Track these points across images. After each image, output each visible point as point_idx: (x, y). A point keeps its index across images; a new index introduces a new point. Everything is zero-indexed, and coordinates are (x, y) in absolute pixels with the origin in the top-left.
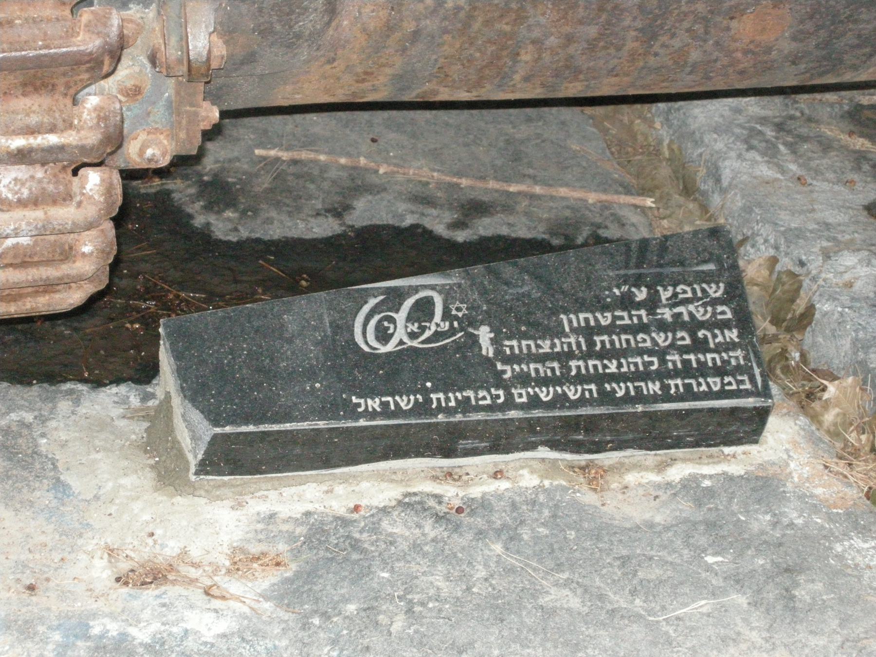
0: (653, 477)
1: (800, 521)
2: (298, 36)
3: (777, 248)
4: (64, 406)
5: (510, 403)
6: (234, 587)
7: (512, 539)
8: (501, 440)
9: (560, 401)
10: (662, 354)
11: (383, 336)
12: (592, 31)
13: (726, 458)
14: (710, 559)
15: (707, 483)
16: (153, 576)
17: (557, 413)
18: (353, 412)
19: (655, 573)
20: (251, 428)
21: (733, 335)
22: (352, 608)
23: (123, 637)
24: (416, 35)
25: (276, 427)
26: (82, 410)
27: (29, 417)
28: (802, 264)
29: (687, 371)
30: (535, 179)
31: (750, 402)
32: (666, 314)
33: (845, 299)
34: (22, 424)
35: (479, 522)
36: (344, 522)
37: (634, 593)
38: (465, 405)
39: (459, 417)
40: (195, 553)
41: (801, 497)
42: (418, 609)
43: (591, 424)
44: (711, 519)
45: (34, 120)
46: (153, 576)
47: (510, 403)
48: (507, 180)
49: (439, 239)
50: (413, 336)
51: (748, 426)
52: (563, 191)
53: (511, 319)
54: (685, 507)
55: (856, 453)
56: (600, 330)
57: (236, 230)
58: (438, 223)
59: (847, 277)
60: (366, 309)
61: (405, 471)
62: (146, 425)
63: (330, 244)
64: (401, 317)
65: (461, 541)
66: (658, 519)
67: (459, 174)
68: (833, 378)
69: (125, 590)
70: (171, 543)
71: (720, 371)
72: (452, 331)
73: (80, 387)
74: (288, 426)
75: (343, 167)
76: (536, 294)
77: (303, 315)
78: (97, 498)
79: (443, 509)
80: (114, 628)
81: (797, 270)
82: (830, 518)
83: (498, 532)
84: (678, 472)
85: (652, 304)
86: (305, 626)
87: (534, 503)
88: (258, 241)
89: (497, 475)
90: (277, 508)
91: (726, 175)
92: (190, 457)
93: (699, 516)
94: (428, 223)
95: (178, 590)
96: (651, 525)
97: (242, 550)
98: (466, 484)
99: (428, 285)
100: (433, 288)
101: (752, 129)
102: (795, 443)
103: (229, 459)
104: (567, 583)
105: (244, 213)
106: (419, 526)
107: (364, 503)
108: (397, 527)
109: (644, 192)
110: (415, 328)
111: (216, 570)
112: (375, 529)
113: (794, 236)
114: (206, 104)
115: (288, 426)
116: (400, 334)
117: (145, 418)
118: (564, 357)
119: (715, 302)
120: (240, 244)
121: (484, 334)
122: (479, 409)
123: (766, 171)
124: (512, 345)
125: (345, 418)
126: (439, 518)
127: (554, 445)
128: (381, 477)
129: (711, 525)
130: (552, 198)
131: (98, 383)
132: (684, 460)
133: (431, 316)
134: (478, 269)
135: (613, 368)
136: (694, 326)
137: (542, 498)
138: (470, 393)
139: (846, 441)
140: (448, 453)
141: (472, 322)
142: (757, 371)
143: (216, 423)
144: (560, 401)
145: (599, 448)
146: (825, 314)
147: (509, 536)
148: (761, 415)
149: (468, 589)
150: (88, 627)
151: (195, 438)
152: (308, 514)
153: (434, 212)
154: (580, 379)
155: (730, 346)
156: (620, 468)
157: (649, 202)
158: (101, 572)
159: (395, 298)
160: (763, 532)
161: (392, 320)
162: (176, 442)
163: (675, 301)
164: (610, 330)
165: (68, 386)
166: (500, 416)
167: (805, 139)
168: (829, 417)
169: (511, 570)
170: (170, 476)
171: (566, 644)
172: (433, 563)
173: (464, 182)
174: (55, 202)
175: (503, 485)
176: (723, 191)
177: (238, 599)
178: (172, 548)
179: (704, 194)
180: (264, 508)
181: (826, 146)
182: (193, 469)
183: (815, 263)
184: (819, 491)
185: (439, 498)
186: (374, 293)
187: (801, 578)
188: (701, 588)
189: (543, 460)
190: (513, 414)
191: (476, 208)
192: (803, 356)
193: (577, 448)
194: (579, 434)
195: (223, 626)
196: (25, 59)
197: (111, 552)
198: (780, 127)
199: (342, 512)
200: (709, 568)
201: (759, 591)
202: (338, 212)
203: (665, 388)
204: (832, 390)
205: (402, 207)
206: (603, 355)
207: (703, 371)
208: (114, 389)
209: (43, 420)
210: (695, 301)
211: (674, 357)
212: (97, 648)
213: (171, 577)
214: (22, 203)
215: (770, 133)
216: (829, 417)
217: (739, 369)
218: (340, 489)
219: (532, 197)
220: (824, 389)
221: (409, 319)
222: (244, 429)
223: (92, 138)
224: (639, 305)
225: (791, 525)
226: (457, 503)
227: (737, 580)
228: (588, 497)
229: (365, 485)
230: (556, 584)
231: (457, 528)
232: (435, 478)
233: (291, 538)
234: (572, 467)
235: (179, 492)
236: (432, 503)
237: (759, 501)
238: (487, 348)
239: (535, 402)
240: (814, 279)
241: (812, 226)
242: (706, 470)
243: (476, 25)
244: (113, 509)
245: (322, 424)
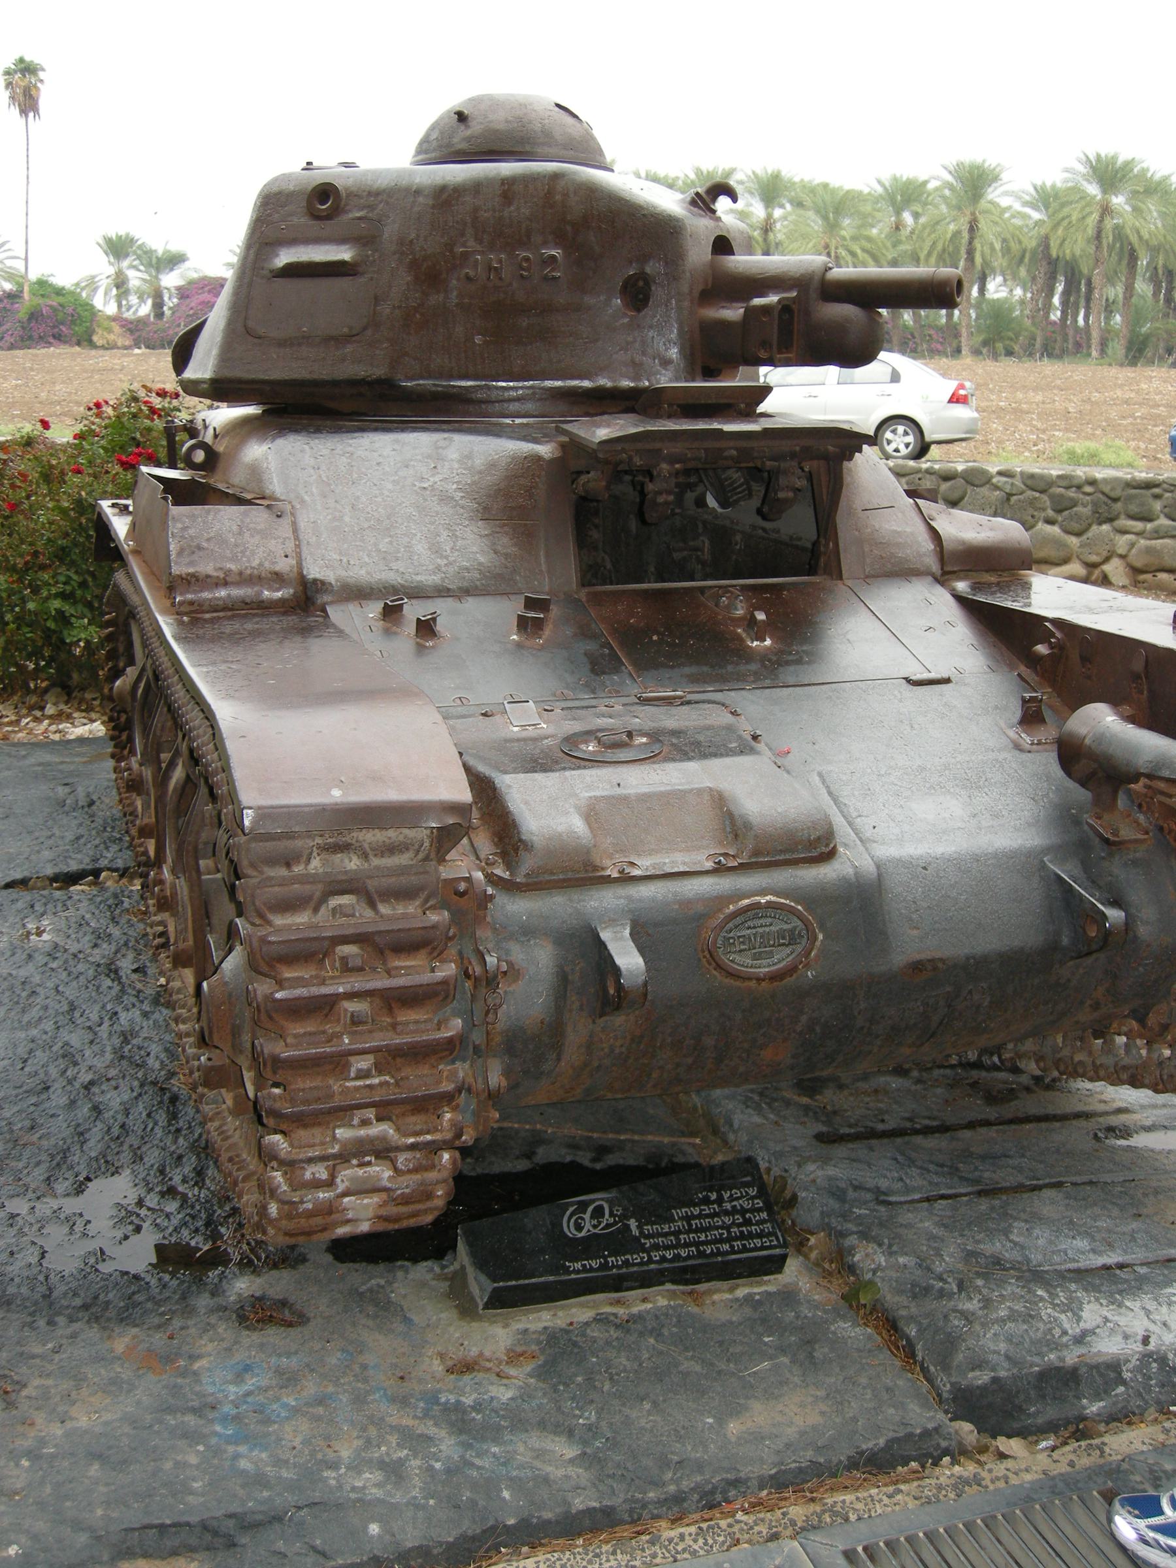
0: (728, 1296)
1: (810, 1315)
2: (542, 1073)
3: (770, 1162)
4: (400, 1274)
5: (650, 1261)
6: (512, 1372)
7: (659, 1336)
8: (646, 1280)
9: (677, 1257)
10: (728, 1228)
11: (579, 1228)
12: (690, 1060)
13: (766, 1283)
14: (766, 1339)
15: (757, 1297)
16: (466, 1367)
17: (677, 1265)
18: (567, 1271)
19: (738, 1349)
20: (514, 1283)
21: (764, 1215)
22: (580, 1379)
23: (458, 1402)
24: (599, 1067)
25: (527, 1282)
26: (410, 1276)
27: (382, 1282)
28: (786, 1171)
29: (742, 1237)
30: (634, 1132)
31: (777, 1251)
32: (728, 1206)
33: (813, 1189)
34: (378, 1285)
35: (639, 1327)
36: (567, 1332)
37: (728, 1360)
38: (626, 1263)
39: (624, 1270)
40: (487, 1353)
41: (808, 1302)
42: (616, 1377)
43: (693, 1269)
44: (763, 1315)
45: (418, 1128)
46: (466, 1367)
47: (650, 1261)
48: (618, 1133)
49: (587, 1168)
50: (595, 1227)
51: (776, 1265)
52: (650, 1138)
53: (646, 1214)
54: (748, 1311)
55: (830, 1274)
56: (694, 1217)
57: (474, 1169)
58: (584, 1159)
59: (812, 1176)
60: (568, 1213)
61: (594, 1301)
62: (448, 1283)
63: (526, 1174)
64: (587, 1216)
65: (632, 1338)
66: (734, 1319)
67: (592, 1131)
68: (812, 1234)
69: (452, 1376)
70: (474, 1349)
71: (760, 1235)
72: (615, 1223)
73: (406, 1263)
74: (533, 1280)
75: (527, 1130)
76: (658, 1200)
77: (535, 1218)
78: (428, 1325)
79: (618, 1321)
80: (452, 1399)
81: (784, 1174)
82: (826, 1312)
83: (651, 1332)
84: (741, 1292)
85: (720, 1201)
86: (556, 1391)
87: (667, 1315)
88: (487, 1175)
89: (644, 1300)
90: (529, 1326)
91: (736, 1125)
92: (479, 1300)
93: (756, 1316)
94: (579, 1160)
95: (481, 1375)
96: (731, 1323)
97: (513, 1351)
98: (628, 1307)
99: (599, 1198)
100: (602, 1199)
101: (746, 1096)
102: (800, 1272)
103: (501, 1301)
104: (693, 1358)
105: (477, 1159)
106: (607, 1331)
107: (575, 1320)
108: (594, 1332)
109: (693, 1134)
110: (595, 1222)
111: (500, 1363)
112: (584, 1335)
113: (779, 1155)
114: (492, 1111)
115: (533, 1280)
116: (588, 1226)
117: (446, 1279)
118: (676, 1234)
119: (753, 1198)
120: (478, 1177)
121: (633, 1224)
122: (634, 1265)
123: (757, 1119)
124: (648, 1228)
125: (563, 1274)
126: (617, 1326)
127: (674, 1282)
128: (582, 1305)
129: (764, 1321)
130: (644, 1141)
131: (415, 1260)
132: (744, 1285)
133: (603, 1215)
134: (625, 1188)
135: (703, 1238)
136: (743, 1212)
137: (670, 1312)
138: (629, 1257)
139: (824, 1268)
140: (618, 1290)
141: (624, 1217)
142: (779, 1234)
143: (494, 1281)
144: (677, 1257)
145: (698, 1282)
146: (803, 1198)
147: (657, 1333)
148: (783, 1259)
149: (640, 1365)
150: (438, 1399)
151: (481, 1290)
152: (545, 1328)
153: (581, 1153)
154: (687, 1245)
155: (763, 1222)
156: (710, 1292)
157: (698, 1141)
158: (438, 1367)
159: (583, 1207)
160: (792, 1322)
161: (583, 1219)
162: (470, 1293)
163: (732, 1199)
164: (699, 1217)
165: (399, 1263)
166: (646, 1268)
167: (776, 1100)
168: (814, 1255)
169: (661, 1353)
170: (467, 1311)
171: (698, 1391)
172: (619, 1351)
173: (595, 1135)
174: (426, 1170)
175: (649, 1306)
176: (735, 1132)
177: (515, 1378)
178: (474, 1351)
179: (724, 1133)
180: (521, 1326)
181: (788, 1103)
182: (481, 1307)
183: (793, 1170)
184: (816, 1297)
185: (615, 1315)
186: (572, 1204)
187: (817, 1346)
188: (765, 1356)
189: (668, 1290)
190: (652, 1266)
191: (602, 1150)
192: (793, 1222)
193: (686, 1282)
194: (687, 1275)
195: (509, 1394)
196: (417, 1097)
197: (442, 1356)
198: (761, 1094)
199: (564, 1326)
200: (766, 1344)
201: (795, 1355)
202: (529, 1156)
203: (732, 1247)
204: (813, 1240)
205: (563, 1151)
206: (698, 1230)
207: (751, 1236)
208: (425, 1264)
209: (390, 1283)
210: (743, 1198)
211: (734, 1230)
212: (445, 1410)
213: (476, 1367)
214: (410, 1171)
215: (756, 1098)
216: (814, 1255)
217: (769, 1234)
218: (560, 1314)
219: (633, 1141)
220: (808, 1240)
221: (592, 1217)
222: (510, 1283)
223: (448, 1136)
224: (713, 1202)
225: (806, 1317)
226: (626, 1317)
227: (782, 1350)
228: (695, 1310)
229: (574, 1310)
230: (686, 1359)
231: (628, 1331)
232: (611, 1304)
233: (539, 1343)
234: (683, 1293)
235: (473, 1320)
236: (612, 1318)
237: (787, 1305)
238: (635, 1231)
239: (663, 1259)
240: (795, 1179)
241: (787, 1149)
242: (756, 1290)
243: (631, 1061)
244: (439, 1332)
245: (551, 1278)
